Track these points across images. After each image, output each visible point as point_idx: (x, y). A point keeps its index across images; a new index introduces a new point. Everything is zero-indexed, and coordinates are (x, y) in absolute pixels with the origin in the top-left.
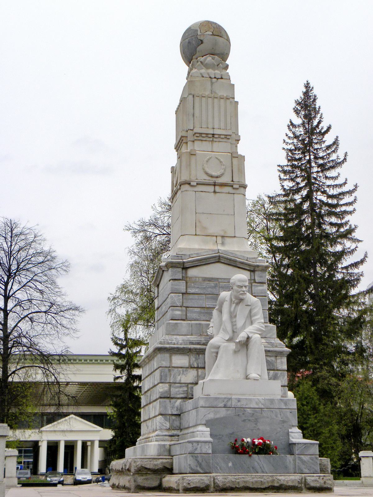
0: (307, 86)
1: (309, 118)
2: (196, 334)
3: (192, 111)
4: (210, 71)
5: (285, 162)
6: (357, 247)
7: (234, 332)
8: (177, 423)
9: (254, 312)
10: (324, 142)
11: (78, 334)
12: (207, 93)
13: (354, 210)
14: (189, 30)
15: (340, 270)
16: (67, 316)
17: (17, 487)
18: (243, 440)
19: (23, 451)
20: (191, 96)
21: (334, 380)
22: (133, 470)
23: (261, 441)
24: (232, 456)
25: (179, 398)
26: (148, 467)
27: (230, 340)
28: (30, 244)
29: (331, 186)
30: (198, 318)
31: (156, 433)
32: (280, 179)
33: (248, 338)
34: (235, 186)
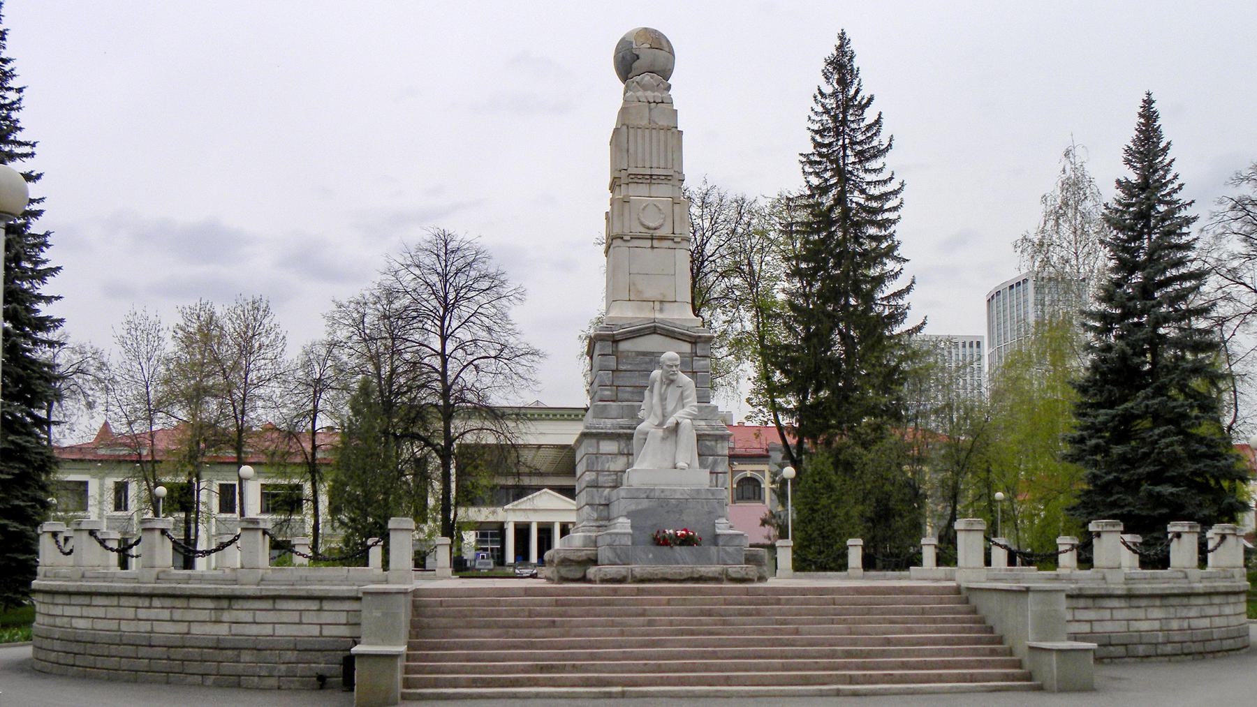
0: (842, 37)
1: (843, 83)
2: (627, 417)
3: (626, 145)
4: (650, 94)
5: (809, 148)
6: (902, 269)
7: (664, 416)
8: (605, 513)
9: (686, 393)
10: (863, 119)
11: (540, 387)
12: (645, 122)
13: (899, 217)
14: (623, 41)
15: (879, 302)
16: (524, 362)
17: (451, 579)
18: (665, 532)
19: (789, 483)
20: (625, 127)
21: (858, 450)
22: (556, 561)
23: (684, 532)
24: (653, 548)
25: (607, 487)
26: (572, 558)
27: (660, 425)
28: (469, 264)
29: (871, 182)
30: (630, 398)
31: (584, 523)
32: (804, 172)
33: (677, 424)
34: (676, 240)
